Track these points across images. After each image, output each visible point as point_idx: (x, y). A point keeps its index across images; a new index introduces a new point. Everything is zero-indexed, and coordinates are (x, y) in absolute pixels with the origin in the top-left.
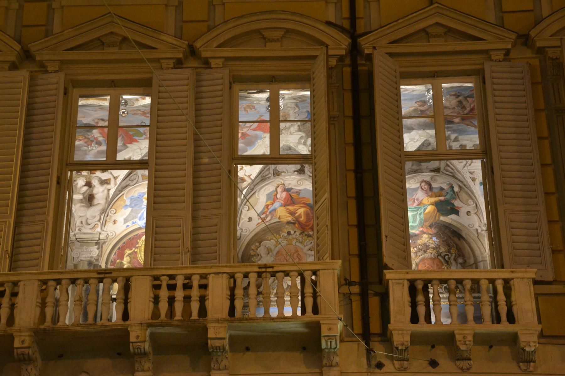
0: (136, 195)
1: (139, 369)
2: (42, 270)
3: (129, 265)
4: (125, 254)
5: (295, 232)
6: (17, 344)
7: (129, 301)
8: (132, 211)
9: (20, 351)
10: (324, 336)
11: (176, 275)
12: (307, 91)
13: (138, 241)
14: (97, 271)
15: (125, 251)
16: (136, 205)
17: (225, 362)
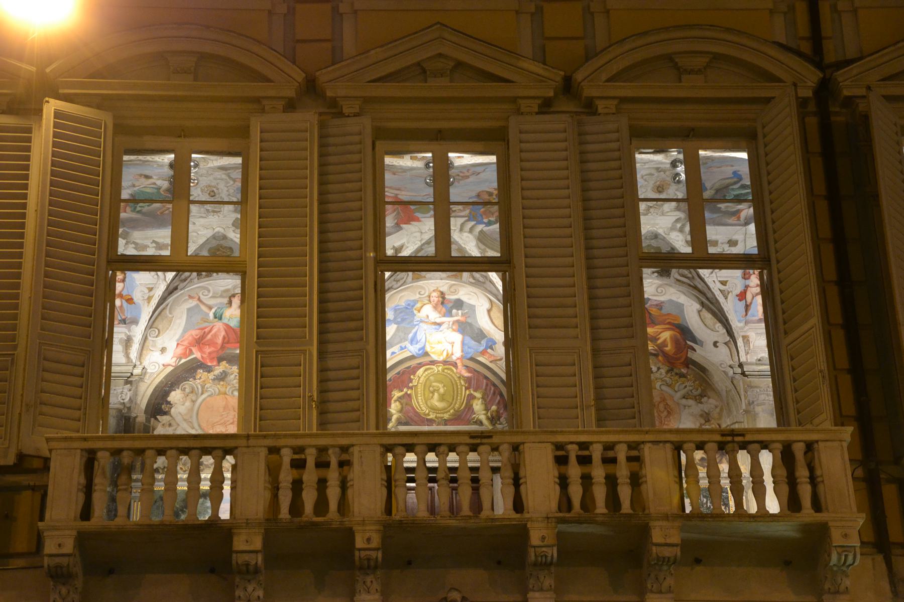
0: (403, 304)
1: (535, 588)
2: (367, 430)
3: (400, 414)
4: (392, 398)
5: (659, 369)
6: (359, 543)
7: (521, 481)
8: (398, 330)
9: (363, 554)
10: (836, 546)
11: (591, 443)
12: (743, 151)
13: (412, 377)
14: (469, 434)
15: (393, 393)
16: (403, 320)
17: (670, 581)
